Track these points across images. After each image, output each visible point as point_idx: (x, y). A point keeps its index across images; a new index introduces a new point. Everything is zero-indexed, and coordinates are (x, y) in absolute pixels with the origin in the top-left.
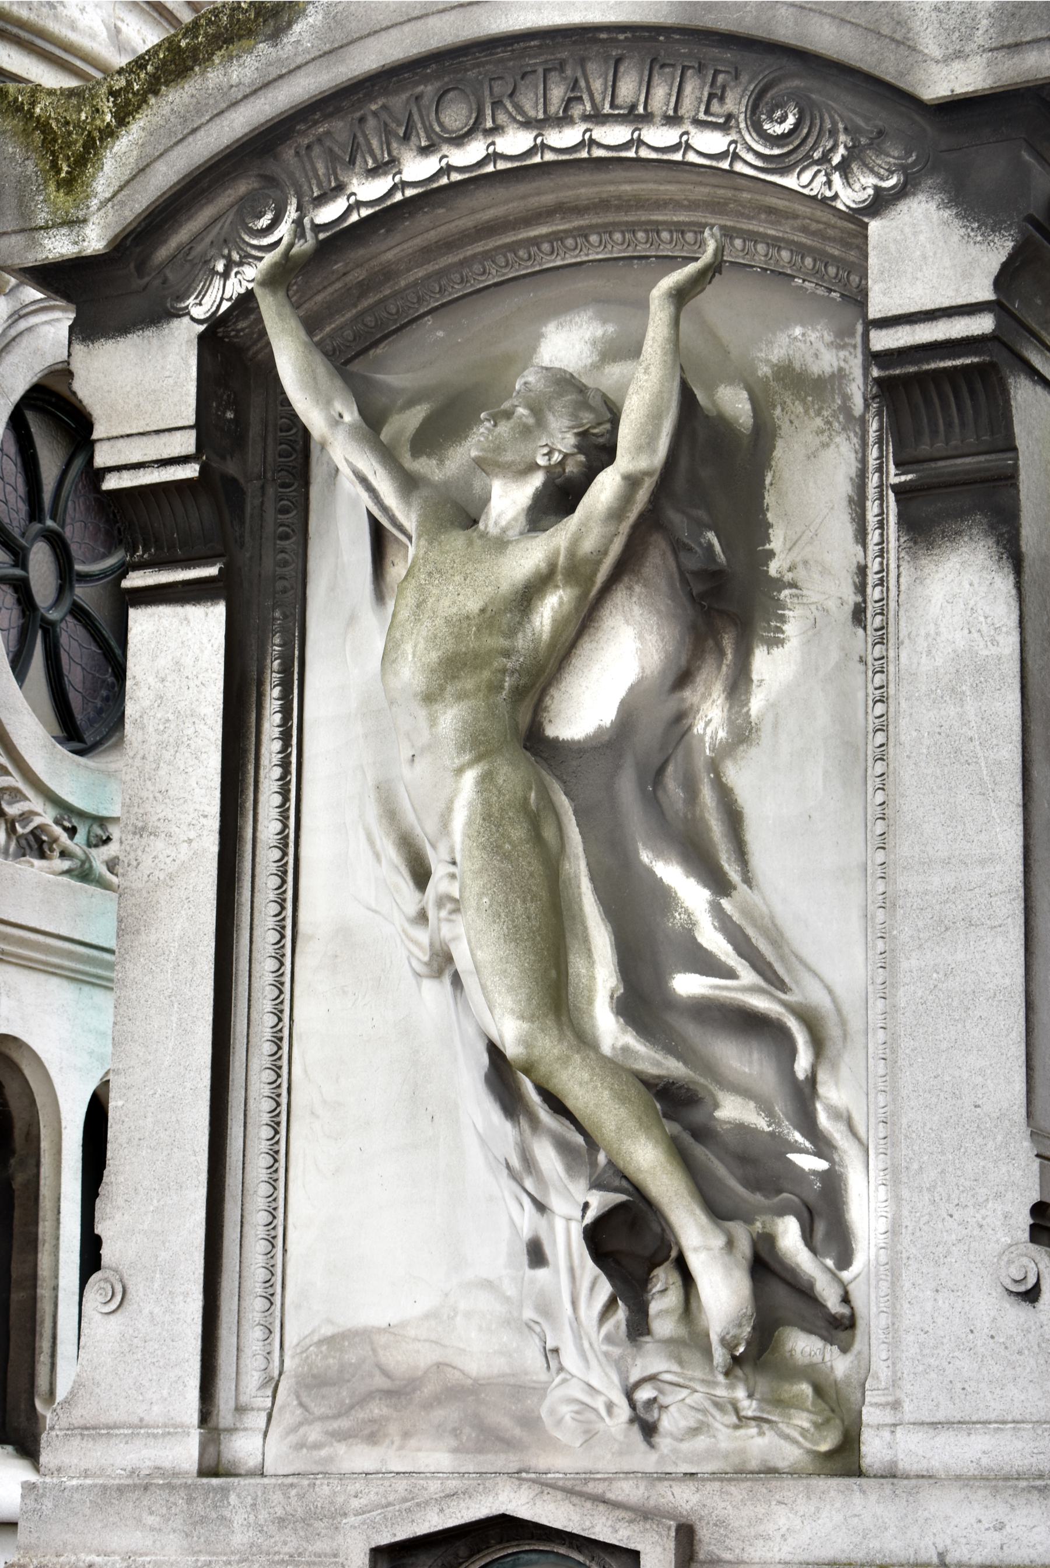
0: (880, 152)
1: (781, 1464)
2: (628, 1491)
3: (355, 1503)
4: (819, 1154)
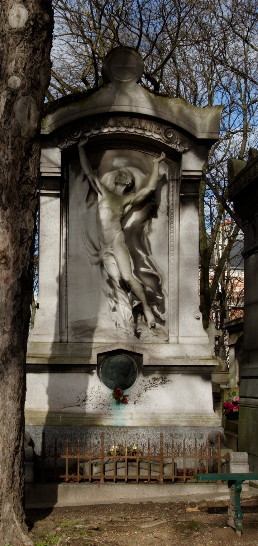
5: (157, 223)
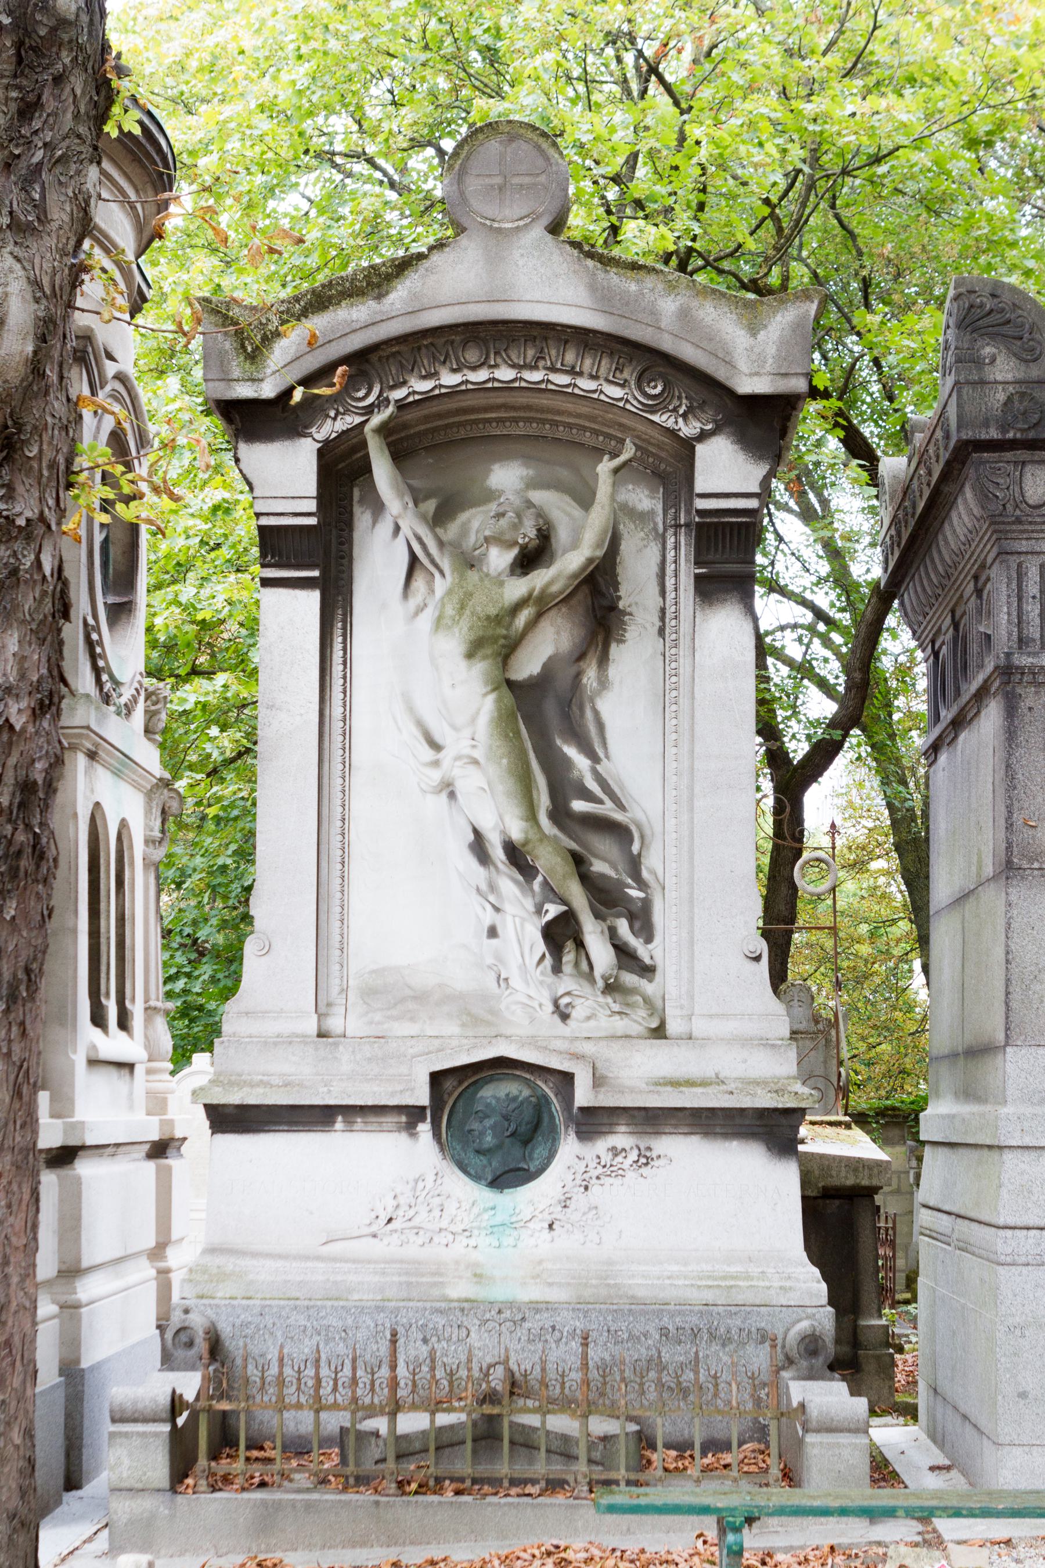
0: (703, 411)
1: (633, 1034)
2: (559, 1045)
3: (411, 1051)
4: (640, 890)
5: (632, 660)
